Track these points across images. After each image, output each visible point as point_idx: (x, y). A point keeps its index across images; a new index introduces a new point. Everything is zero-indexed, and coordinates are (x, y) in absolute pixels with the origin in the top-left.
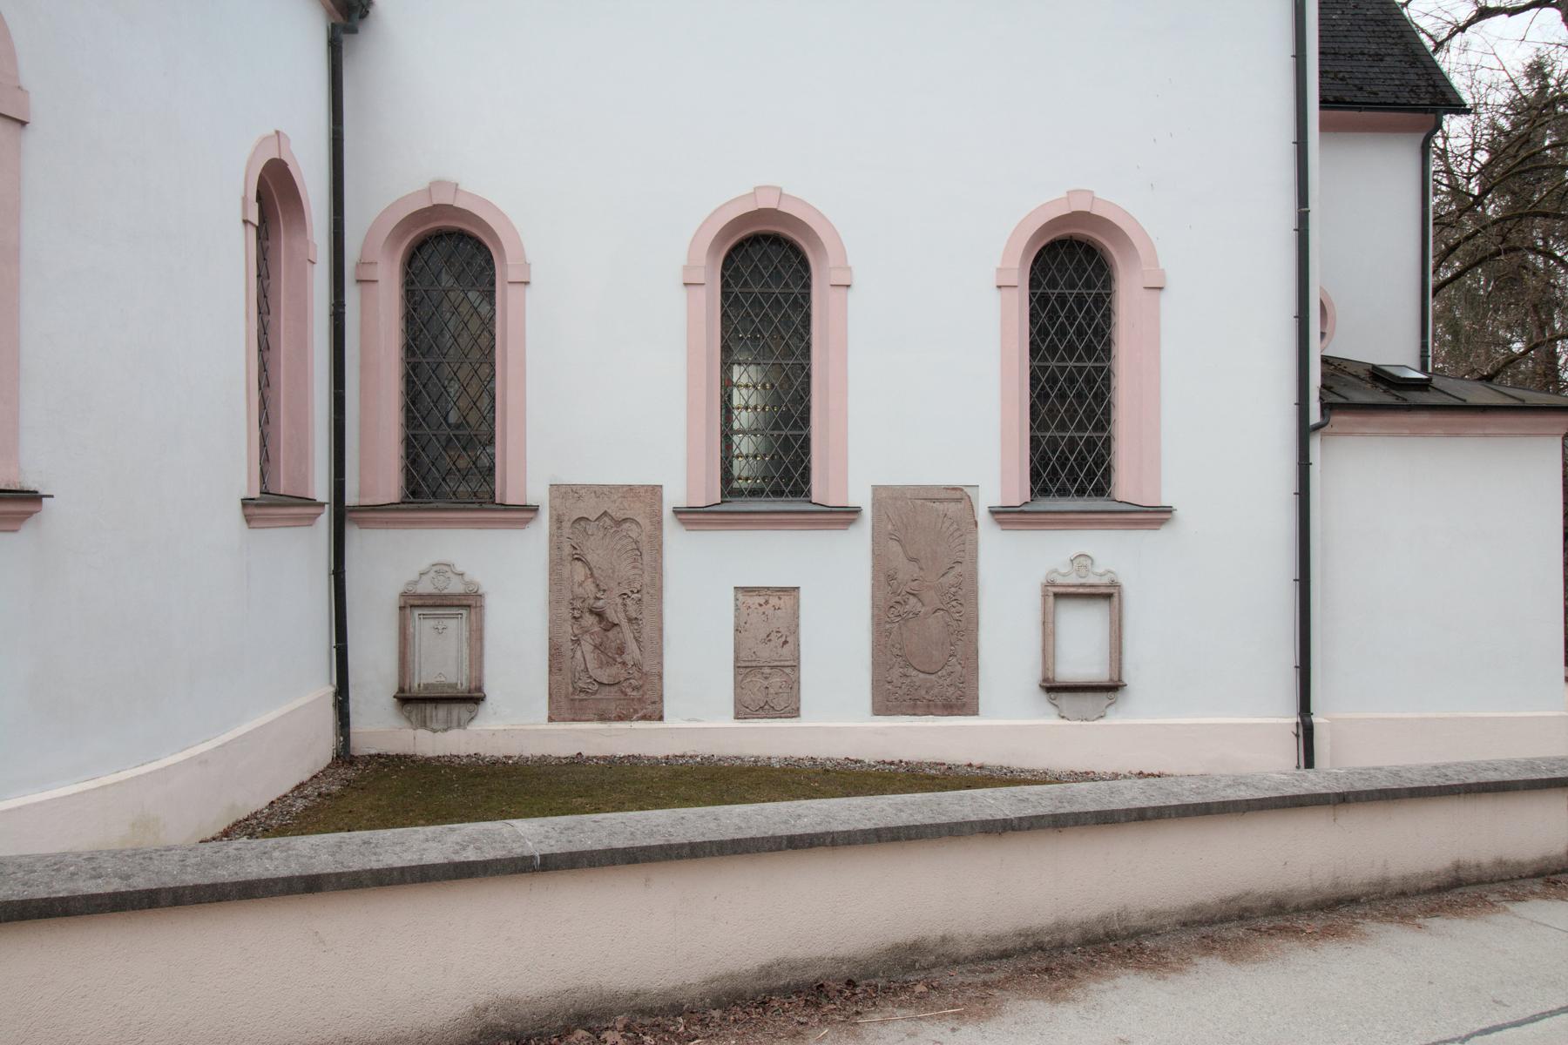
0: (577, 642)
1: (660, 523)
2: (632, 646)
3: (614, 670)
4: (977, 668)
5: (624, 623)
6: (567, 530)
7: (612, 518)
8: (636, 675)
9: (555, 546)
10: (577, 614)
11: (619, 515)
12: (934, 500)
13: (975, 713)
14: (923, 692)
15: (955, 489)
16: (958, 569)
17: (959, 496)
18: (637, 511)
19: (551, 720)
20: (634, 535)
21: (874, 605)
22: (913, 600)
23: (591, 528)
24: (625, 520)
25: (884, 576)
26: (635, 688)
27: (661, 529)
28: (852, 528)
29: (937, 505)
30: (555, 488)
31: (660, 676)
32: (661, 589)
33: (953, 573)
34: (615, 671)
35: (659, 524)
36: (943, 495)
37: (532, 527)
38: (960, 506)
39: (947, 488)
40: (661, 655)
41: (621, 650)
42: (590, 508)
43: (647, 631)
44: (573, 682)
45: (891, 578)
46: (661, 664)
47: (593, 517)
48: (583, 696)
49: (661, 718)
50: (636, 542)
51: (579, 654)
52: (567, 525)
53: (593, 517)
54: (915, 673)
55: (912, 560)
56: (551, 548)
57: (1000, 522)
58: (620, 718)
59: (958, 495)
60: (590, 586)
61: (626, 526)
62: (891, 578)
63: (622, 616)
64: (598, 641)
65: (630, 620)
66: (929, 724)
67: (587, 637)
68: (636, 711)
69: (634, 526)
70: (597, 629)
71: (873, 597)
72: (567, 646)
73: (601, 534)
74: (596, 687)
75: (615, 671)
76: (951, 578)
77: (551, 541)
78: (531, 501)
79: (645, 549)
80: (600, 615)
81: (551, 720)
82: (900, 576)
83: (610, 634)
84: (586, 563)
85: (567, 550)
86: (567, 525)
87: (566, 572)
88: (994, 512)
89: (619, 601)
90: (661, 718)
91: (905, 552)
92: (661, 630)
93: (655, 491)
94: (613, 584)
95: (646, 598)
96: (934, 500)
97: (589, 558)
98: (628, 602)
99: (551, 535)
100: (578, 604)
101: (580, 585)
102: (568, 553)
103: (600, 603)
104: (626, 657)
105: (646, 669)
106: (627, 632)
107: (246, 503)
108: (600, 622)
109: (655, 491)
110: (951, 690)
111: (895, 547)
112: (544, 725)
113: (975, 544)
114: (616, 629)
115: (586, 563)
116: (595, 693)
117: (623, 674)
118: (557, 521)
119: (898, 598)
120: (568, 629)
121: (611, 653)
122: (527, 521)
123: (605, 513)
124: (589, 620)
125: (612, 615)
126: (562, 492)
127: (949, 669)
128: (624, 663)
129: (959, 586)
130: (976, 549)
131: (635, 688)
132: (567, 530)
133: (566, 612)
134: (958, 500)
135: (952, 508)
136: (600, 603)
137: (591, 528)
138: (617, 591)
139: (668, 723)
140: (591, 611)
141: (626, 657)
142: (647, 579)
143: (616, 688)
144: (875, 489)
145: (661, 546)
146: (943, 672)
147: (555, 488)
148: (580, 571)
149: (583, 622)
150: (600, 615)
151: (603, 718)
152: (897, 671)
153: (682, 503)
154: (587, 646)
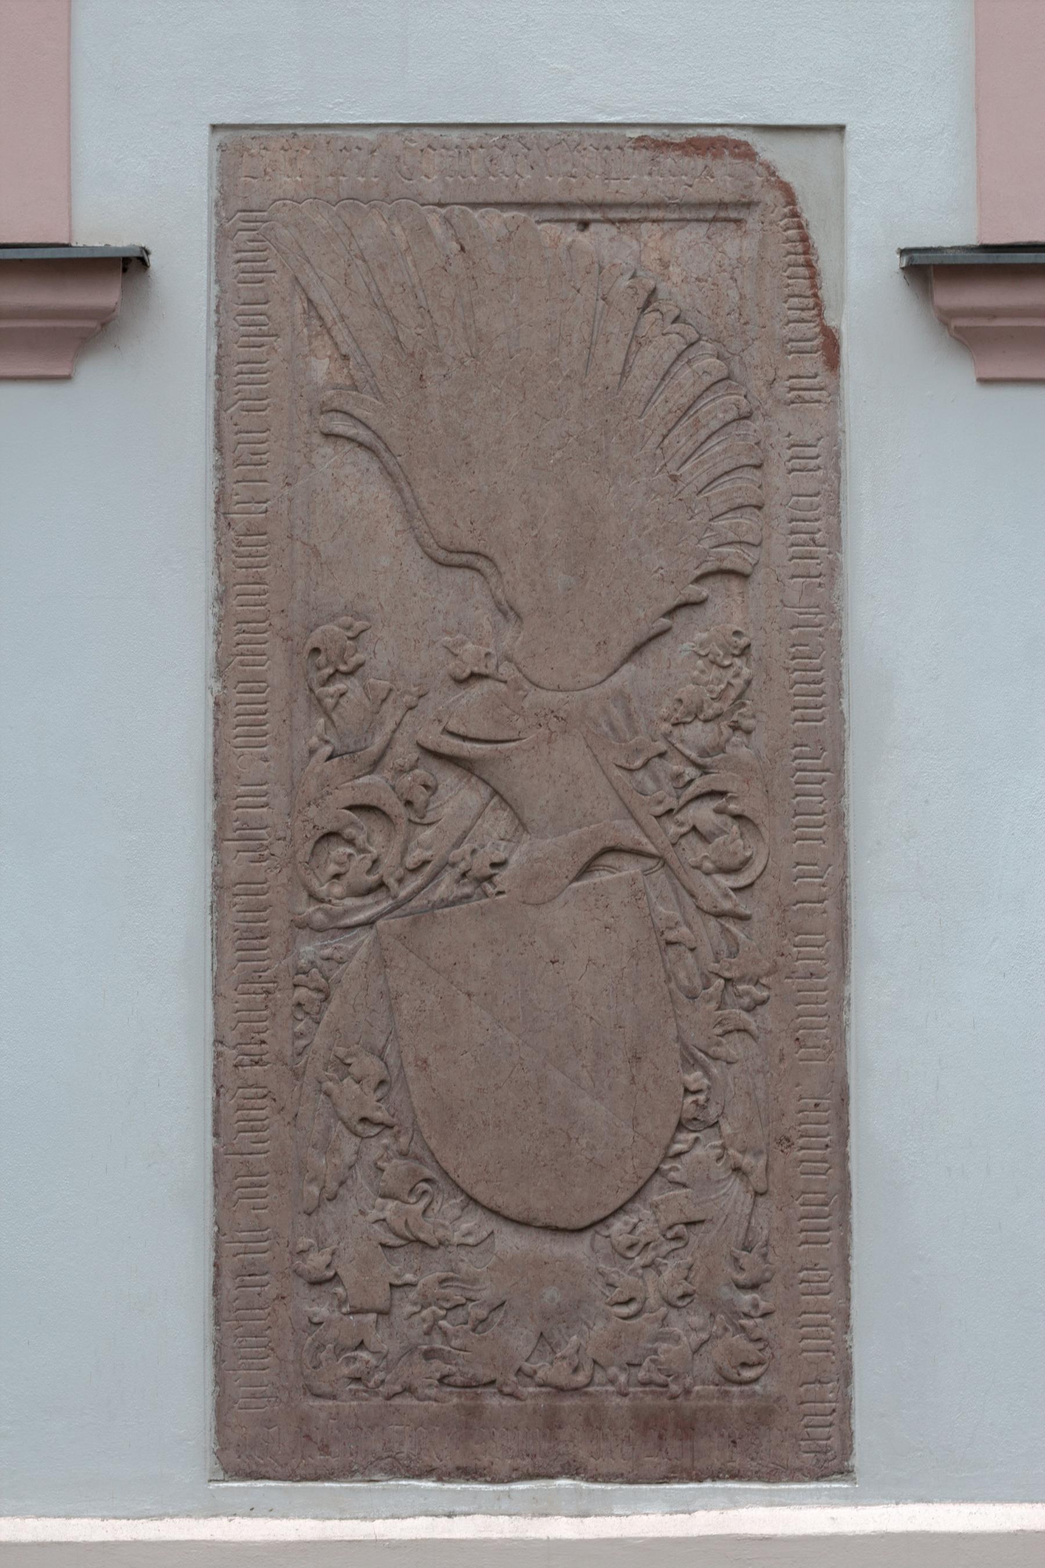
4: (842, 1196)
12: (584, 213)
13: (824, 1457)
14: (520, 1341)
15: (706, 144)
16: (727, 610)
17: (729, 184)
21: (232, 827)
22: (457, 798)
25: (286, 662)
28: (97, 378)
29: (599, 239)
33: (695, 633)
36: (637, 180)
38: (735, 245)
39: (661, 142)
45: (328, 666)
54: (472, 1223)
55: (455, 558)
57: (968, 336)
58: (365, 1518)
59: (722, 179)
62: (328, 666)
66: (562, 1528)
71: (221, 775)
76: (680, 667)
82: (381, 654)
88: (927, 270)
91: (411, 514)
96: (584, 213)
107: (148, 253)
110: (688, 1325)
111: (351, 485)
113: (824, 466)
119: (375, 786)
126: (268, 177)
127: (670, 1202)
129: (733, 715)
130: (831, 499)
134: (725, 213)
135: (685, 256)
146: (644, 1220)
152: (362, 1218)
153: (954, 230)
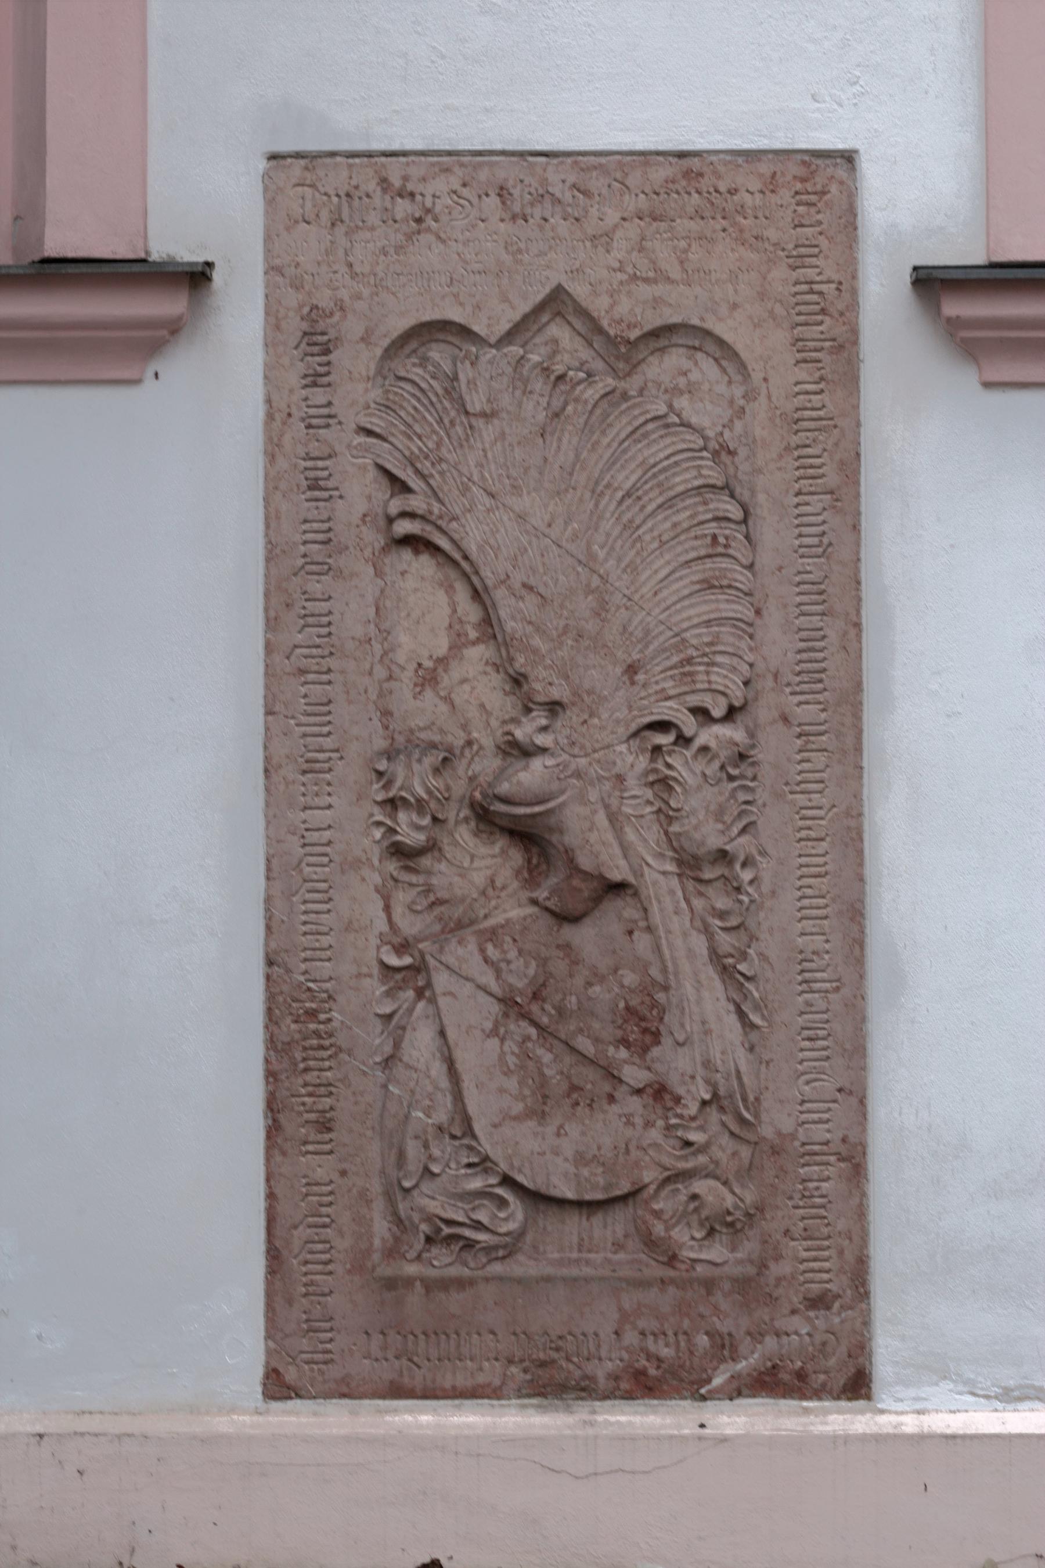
0: (411, 976)
1: (846, 347)
2: (702, 1001)
3: (606, 1129)
5: (660, 880)
6: (355, 387)
7: (593, 328)
8: (724, 1150)
9: (298, 473)
10: (410, 830)
11: (630, 310)
18: (728, 289)
19: (278, 1386)
20: (705, 414)
23: (483, 379)
24: (661, 335)
26: (718, 1225)
27: (850, 379)
30: (292, 169)
31: (854, 1162)
32: (851, 700)
34: (608, 1136)
35: (833, 350)
37: (178, 371)
40: (856, 1051)
41: (644, 1024)
42: (475, 275)
43: (782, 925)
44: (396, 1192)
46: (855, 1096)
47: (492, 319)
48: (443, 1262)
49: (858, 1386)
50: (722, 452)
51: (420, 1045)
52: (356, 362)
53: (492, 319)
56: (273, 486)
57: (969, 344)
58: (643, 1384)
60: (478, 686)
61: (664, 367)
63: (646, 837)
64: (521, 975)
65: (689, 864)
67: (464, 953)
68: (725, 1347)
69: (706, 370)
70: (513, 910)
72: (359, 1001)
73: (534, 410)
74: (516, 1213)
75: (608, 1136)
77: (272, 450)
78: (169, 243)
79: (771, 483)
80: (528, 836)
81: (278, 1386)
83: (584, 937)
84: (457, 564)
85: (359, 493)
86: (356, 362)
87: (353, 615)
88: (930, 283)
89: (633, 761)
90: (858, 1386)
92: (855, 912)
93: (822, 180)
94: (599, 674)
95: (774, 747)
97: (473, 535)
98: (682, 765)
99: (275, 416)
100: (416, 778)
101: (428, 678)
102: (367, 505)
103: (532, 775)
104: (676, 1063)
105: (777, 1119)
106: (675, 925)
108: (531, 876)
109: (822, 180)
112: (242, 1411)
114: (617, 912)
115: (457, 564)
116: (510, 1247)
117: (655, 1151)
118: (309, 341)
120: (365, 910)
121: (594, 1040)
122: (155, 341)
123: (556, 302)
124: (476, 864)
125: (595, 839)
126: (328, 189)
128: (659, 1093)
131: (718, 1225)
132: (355, 387)
133: (352, 823)
136: (532, 775)
137: (483, 379)
138: (620, 710)
139: (906, 1410)
140: (485, 817)
141: (676, 1063)
142: (777, 644)
143: (616, 1224)
144: (915, 269)
145: (850, 467)
147: (292, 169)
148: (424, 605)
149: (443, 876)
150: (528, 836)
151: (552, 1381)
154: (465, 1000)
